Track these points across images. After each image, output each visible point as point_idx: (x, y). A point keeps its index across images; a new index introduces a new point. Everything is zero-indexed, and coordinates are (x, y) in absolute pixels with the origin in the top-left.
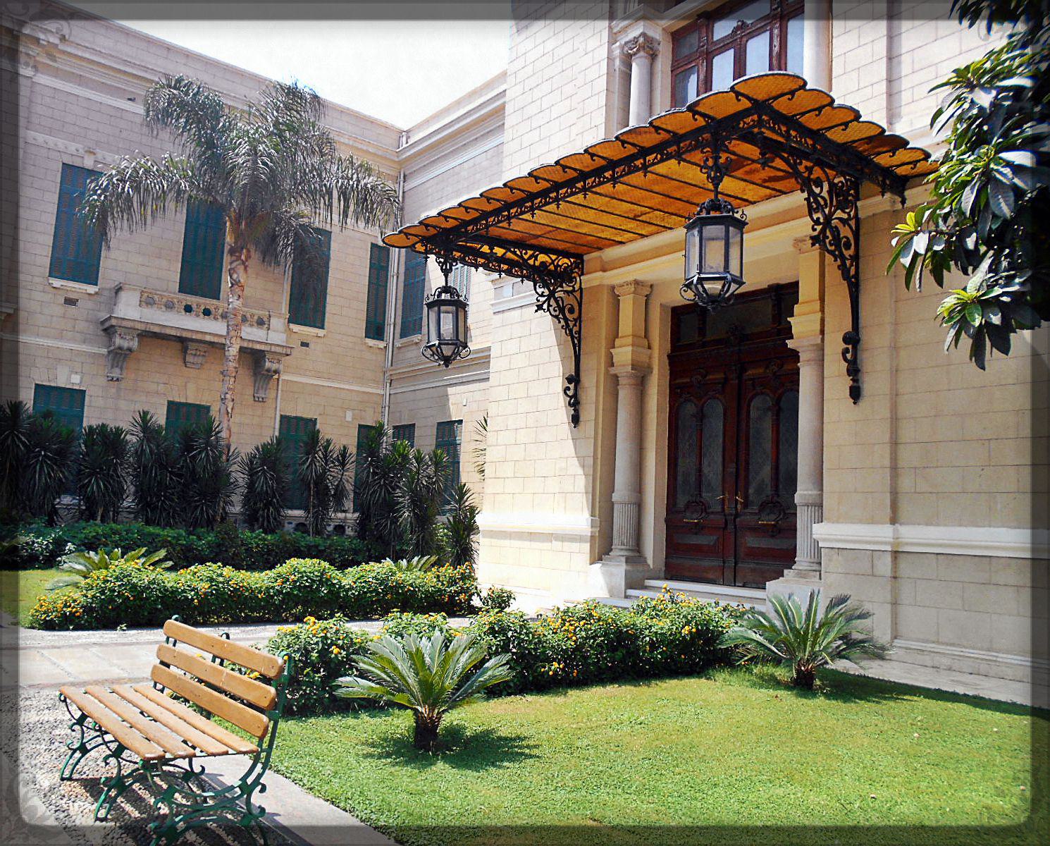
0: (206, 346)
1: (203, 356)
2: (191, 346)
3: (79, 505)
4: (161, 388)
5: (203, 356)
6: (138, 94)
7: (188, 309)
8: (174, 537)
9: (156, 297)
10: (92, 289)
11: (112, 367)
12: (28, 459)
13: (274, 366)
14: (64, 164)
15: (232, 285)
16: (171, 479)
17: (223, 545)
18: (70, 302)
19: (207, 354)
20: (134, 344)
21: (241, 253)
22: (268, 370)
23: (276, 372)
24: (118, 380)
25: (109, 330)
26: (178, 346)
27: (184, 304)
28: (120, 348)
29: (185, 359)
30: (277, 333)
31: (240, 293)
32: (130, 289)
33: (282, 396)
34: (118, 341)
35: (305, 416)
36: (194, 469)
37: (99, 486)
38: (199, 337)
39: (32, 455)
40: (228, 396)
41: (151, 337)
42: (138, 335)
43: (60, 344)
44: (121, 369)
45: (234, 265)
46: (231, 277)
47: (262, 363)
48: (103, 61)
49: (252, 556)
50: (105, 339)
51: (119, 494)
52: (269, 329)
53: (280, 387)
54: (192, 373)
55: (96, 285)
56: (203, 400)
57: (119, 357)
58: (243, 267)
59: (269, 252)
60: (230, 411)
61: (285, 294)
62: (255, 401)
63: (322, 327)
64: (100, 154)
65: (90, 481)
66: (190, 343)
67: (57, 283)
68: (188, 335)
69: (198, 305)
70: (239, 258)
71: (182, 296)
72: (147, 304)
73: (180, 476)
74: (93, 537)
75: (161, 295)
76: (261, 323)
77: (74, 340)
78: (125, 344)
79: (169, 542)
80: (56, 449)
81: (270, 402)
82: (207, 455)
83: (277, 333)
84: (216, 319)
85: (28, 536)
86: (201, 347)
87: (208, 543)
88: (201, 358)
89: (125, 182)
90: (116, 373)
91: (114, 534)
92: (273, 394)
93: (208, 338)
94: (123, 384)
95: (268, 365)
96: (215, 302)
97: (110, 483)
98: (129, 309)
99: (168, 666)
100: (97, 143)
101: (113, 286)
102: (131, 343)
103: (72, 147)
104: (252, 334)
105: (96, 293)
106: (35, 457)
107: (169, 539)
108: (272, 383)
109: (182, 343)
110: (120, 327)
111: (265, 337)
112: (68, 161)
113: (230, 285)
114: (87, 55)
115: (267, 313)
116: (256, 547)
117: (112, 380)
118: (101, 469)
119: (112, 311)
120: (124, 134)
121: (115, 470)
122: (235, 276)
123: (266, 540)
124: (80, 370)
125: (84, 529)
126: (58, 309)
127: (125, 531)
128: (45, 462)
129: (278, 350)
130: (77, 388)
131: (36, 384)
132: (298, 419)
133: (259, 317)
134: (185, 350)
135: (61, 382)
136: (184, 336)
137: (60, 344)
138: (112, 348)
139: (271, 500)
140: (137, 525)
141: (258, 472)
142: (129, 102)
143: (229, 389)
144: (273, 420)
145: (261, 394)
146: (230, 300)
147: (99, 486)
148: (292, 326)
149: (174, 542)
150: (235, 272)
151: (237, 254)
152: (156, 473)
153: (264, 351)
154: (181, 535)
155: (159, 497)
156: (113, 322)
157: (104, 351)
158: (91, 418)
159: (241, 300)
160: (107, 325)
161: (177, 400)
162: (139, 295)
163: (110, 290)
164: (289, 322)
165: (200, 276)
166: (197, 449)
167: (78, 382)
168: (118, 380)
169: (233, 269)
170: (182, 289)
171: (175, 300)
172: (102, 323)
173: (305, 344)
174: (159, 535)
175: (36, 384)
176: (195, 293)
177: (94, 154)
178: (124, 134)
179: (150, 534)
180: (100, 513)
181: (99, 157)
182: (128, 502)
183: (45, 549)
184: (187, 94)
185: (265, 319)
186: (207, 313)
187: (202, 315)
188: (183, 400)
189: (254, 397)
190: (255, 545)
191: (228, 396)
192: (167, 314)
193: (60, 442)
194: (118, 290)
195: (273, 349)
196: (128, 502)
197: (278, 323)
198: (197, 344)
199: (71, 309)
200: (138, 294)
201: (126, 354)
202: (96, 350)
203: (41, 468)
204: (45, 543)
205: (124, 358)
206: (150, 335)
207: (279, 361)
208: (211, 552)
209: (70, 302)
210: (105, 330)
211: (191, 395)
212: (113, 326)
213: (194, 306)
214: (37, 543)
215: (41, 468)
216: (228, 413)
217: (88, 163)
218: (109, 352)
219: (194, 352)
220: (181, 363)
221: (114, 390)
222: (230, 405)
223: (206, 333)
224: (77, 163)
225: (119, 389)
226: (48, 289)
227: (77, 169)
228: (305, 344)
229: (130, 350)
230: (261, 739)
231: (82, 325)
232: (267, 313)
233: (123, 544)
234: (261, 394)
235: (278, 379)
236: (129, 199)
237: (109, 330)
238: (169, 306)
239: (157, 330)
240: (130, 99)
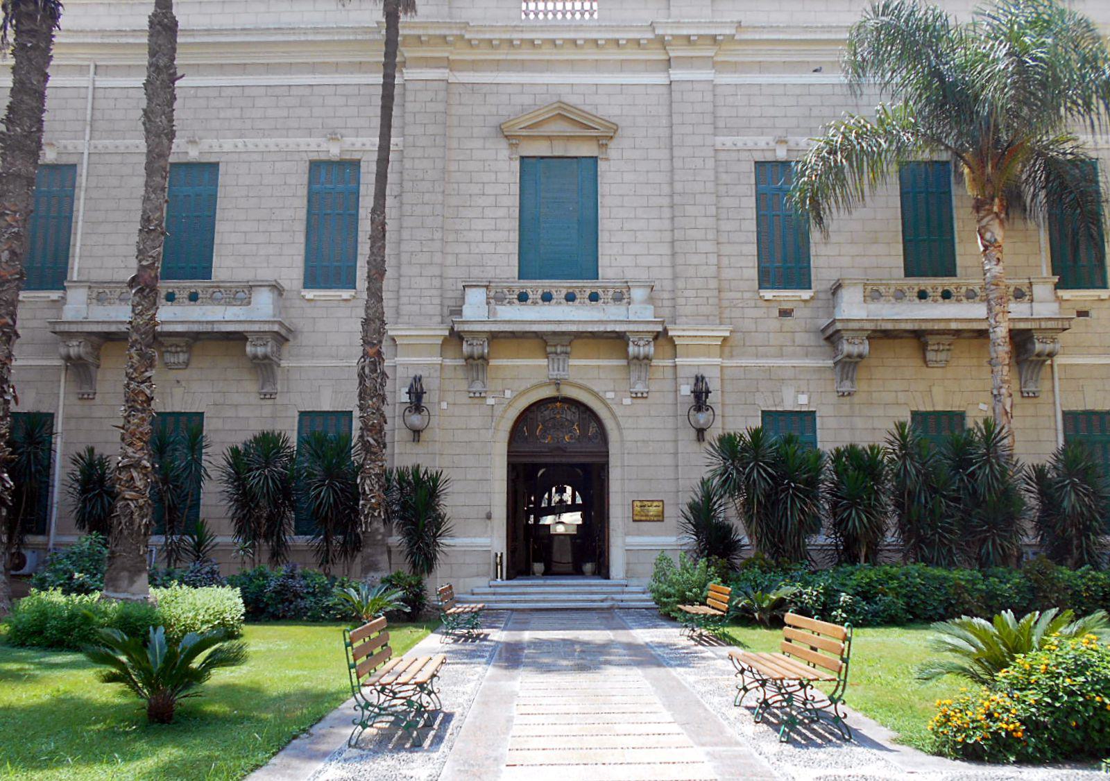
0: (950, 337)
1: (948, 350)
2: (932, 340)
3: (837, 545)
4: (902, 397)
5: (948, 350)
6: (824, 62)
7: (922, 295)
8: (968, 581)
9: (882, 289)
10: (806, 294)
11: (842, 380)
12: (776, 493)
13: (1049, 348)
14: (756, 162)
15: (986, 248)
16: (948, 506)
17: (1039, 589)
18: (785, 313)
19: (952, 347)
20: (865, 348)
21: (992, 205)
22: (1039, 355)
23: (1051, 355)
24: (849, 394)
25: (832, 337)
26: (914, 342)
27: (916, 290)
28: (849, 356)
29: (924, 358)
30: (1045, 304)
31: (999, 255)
32: (849, 285)
33: (1060, 385)
34: (846, 348)
35: (1099, 408)
36: (975, 491)
37: (861, 520)
38: (942, 326)
39: (780, 489)
40: (1003, 391)
41: (882, 336)
42: (868, 338)
43: (780, 362)
44: (852, 381)
45: (984, 222)
46: (982, 238)
47: (1029, 346)
48: (782, 36)
49: (1083, 604)
50: (828, 349)
51: (880, 530)
52: (1032, 301)
53: (1056, 375)
54: (937, 373)
55: (810, 288)
56: (954, 405)
57: (848, 366)
58: (997, 221)
59: (1013, 203)
60: (1009, 410)
61: (1043, 253)
62: (1023, 397)
63: (1104, 287)
64: (792, 140)
65: (850, 514)
66: (930, 337)
67: (768, 294)
68: (924, 326)
69: (935, 288)
70: (990, 211)
71: (912, 281)
72: (873, 299)
73: (957, 500)
74: (867, 584)
75: (888, 285)
76: (1019, 295)
77: (794, 355)
78: (855, 350)
79: (964, 587)
80: (807, 479)
81: (1044, 396)
82: (991, 467)
83: (1045, 304)
84: (959, 301)
85: (794, 585)
86: (946, 339)
87: (1017, 586)
88: (945, 353)
89: (836, 153)
90: (847, 386)
91: (891, 578)
92: (1046, 385)
93: (954, 326)
94: (856, 399)
95: (1038, 347)
96: (953, 280)
97: (872, 514)
98: (853, 308)
99: (815, 649)
100: (787, 130)
101: (829, 286)
102: (861, 347)
103: (762, 141)
104: (1018, 309)
105: (812, 298)
106: (783, 491)
107: (963, 583)
108: (1046, 371)
109: (919, 339)
110: (847, 330)
111: (1029, 312)
112: (759, 157)
113: (982, 249)
114: (765, 36)
115: (1027, 281)
116: (1086, 590)
117: (843, 395)
118: (861, 498)
119: (831, 314)
120: (815, 112)
121: (877, 500)
122: (988, 236)
123: (1098, 579)
124: (805, 389)
125: (852, 573)
126: (774, 323)
127: (903, 575)
128: (798, 496)
129: (1050, 325)
130: (806, 409)
131: (763, 412)
132: (1089, 414)
133: (1016, 289)
134: (923, 348)
135: (788, 406)
136: (923, 328)
137: (780, 362)
138: (839, 357)
139: (1091, 524)
140: (916, 567)
141: (1066, 486)
142: (816, 74)
143: (1003, 382)
144: (1053, 418)
145: (1031, 387)
146: (987, 268)
147: (861, 520)
148: (1061, 293)
149: (969, 586)
150: (988, 230)
151: (987, 207)
152: (926, 499)
153: (1030, 330)
154: (976, 578)
155: (934, 529)
156: (839, 326)
157: (830, 363)
158: (829, 439)
159: (1001, 263)
160: (830, 331)
161: (922, 409)
162: (862, 290)
163: (826, 291)
164: (1056, 289)
165: (928, 251)
166: (976, 463)
167: (806, 402)
168: (849, 394)
169: (983, 227)
170: (909, 272)
171: (905, 287)
172: (823, 331)
173: (1082, 314)
174: (945, 578)
175: (763, 412)
176: (924, 274)
177: (786, 142)
178: (815, 112)
179: (935, 578)
180: (863, 554)
181: (792, 144)
182: (891, 537)
183: (816, 601)
184: (898, 17)
185: (1025, 289)
186: (946, 295)
187: (940, 299)
188: (930, 409)
189: (1022, 392)
190: (1083, 588)
191: (1003, 391)
192: (898, 305)
193: (809, 471)
194: (837, 288)
195: (1044, 325)
196: (891, 537)
197: (1043, 291)
198: (938, 337)
199: (788, 322)
200: (860, 289)
201: (856, 363)
202: (820, 363)
203: (793, 502)
204: (815, 593)
205: (855, 367)
206: (879, 334)
207: (1054, 340)
208: (1023, 598)
209: (785, 313)
210: (828, 339)
211: (940, 402)
212: (838, 331)
213: (929, 290)
214: (806, 593)
215: (793, 502)
216: (1007, 413)
217: (781, 154)
218: (836, 364)
219: (936, 347)
220: (920, 362)
221: (847, 407)
222: (1008, 402)
223: (950, 320)
224: (769, 157)
225: (852, 404)
226: (760, 303)
227: (768, 166)
228: (1082, 314)
229: (860, 356)
230: (839, 673)
231: (801, 338)
232: (1027, 281)
233: (904, 591)
234: (1031, 387)
235: (1052, 366)
236: (841, 169)
237: (832, 337)
238: (900, 295)
239: (889, 326)
240: (815, 71)
